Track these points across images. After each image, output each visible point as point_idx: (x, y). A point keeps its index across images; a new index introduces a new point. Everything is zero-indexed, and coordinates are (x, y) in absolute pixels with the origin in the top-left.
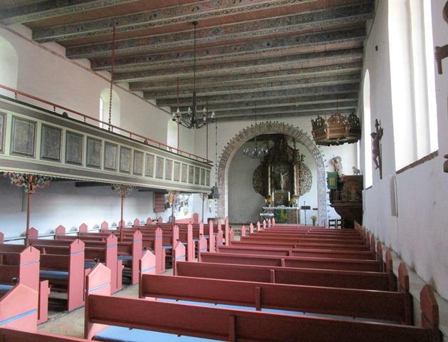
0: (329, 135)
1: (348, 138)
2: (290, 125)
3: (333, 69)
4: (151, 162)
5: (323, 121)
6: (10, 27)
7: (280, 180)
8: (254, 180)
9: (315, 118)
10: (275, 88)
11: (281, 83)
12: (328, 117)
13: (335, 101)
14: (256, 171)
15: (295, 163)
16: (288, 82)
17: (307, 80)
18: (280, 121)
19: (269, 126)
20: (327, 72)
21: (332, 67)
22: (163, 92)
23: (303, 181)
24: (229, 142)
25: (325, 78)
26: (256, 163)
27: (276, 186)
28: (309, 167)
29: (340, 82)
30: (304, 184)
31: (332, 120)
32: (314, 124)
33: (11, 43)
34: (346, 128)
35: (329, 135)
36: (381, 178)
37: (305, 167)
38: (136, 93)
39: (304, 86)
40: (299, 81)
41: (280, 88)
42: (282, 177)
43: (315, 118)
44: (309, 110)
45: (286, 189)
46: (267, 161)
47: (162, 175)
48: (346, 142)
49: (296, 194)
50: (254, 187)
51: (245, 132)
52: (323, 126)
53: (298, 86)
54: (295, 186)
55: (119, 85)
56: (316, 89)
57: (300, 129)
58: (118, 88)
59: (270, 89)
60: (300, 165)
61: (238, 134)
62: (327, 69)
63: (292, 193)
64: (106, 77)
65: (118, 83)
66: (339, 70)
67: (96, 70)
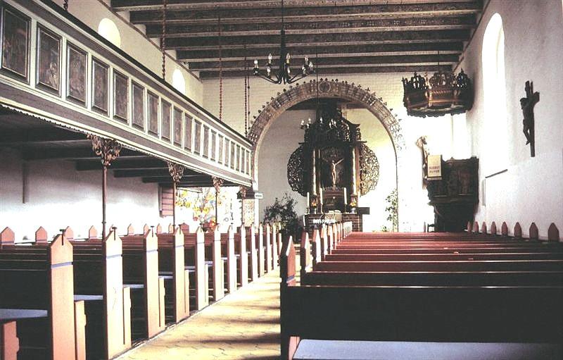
0: (431, 102)
1: (453, 106)
2: (356, 85)
3: (443, 9)
4: (199, 132)
5: (422, 81)
6: (118, 13)
7: (331, 170)
8: (289, 171)
9: (409, 76)
10: (356, 30)
11: (365, 23)
12: (431, 75)
13: (435, 52)
14: (292, 157)
15: (354, 146)
16: (376, 22)
17: (402, 22)
18: (342, 79)
19: (325, 86)
20: (436, 12)
21: (443, 6)
22: (180, 28)
23: (365, 172)
24: (266, 105)
25: (429, 20)
26: (293, 144)
27: (325, 180)
28: (370, 145)
29: (448, 27)
30: (367, 177)
31: (434, 81)
32: (408, 87)
33: (503, 21)
34: (455, 93)
35: (431, 102)
36: (507, 170)
37: (369, 152)
38: (138, 26)
39: (397, 29)
40: (391, 22)
41: (362, 29)
42: (334, 166)
43: (409, 76)
44: (389, 65)
45: (340, 185)
46: (314, 137)
47: (125, 114)
48: (448, 112)
49: (355, 193)
50: (290, 183)
51: (288, 94)
52: (423, 89)
53: (389, 29)
54: (354, 181)
55: (193, 72)
56: (410, 34)
57: (371, 93)
58: (116, 18)
59: (348, 30)
60: (361, 147)
61: (275, 96)
62: (436, 9)
63: (350, 191)
64: (171, 55)
65: (119, 11)
66: (452, 11)
67: (134, 24)
